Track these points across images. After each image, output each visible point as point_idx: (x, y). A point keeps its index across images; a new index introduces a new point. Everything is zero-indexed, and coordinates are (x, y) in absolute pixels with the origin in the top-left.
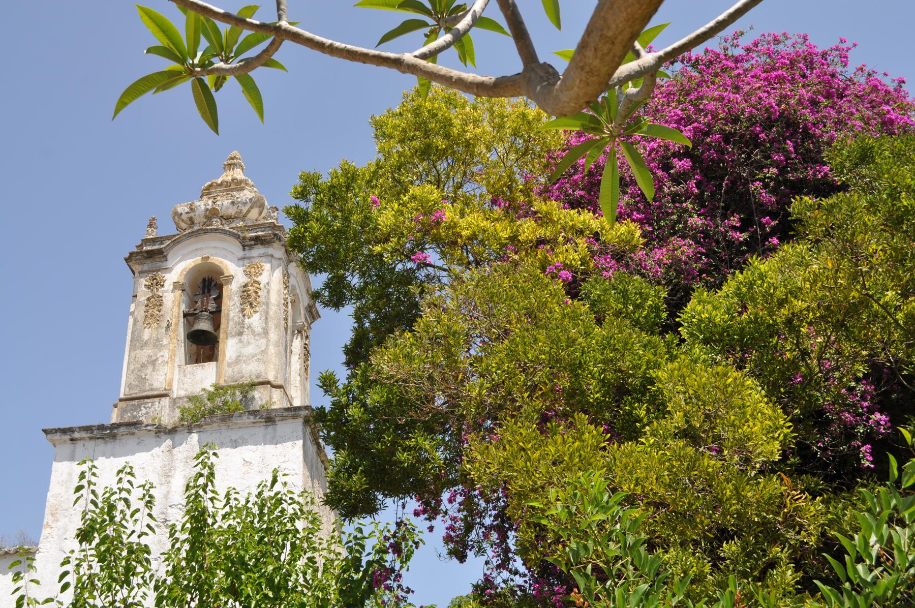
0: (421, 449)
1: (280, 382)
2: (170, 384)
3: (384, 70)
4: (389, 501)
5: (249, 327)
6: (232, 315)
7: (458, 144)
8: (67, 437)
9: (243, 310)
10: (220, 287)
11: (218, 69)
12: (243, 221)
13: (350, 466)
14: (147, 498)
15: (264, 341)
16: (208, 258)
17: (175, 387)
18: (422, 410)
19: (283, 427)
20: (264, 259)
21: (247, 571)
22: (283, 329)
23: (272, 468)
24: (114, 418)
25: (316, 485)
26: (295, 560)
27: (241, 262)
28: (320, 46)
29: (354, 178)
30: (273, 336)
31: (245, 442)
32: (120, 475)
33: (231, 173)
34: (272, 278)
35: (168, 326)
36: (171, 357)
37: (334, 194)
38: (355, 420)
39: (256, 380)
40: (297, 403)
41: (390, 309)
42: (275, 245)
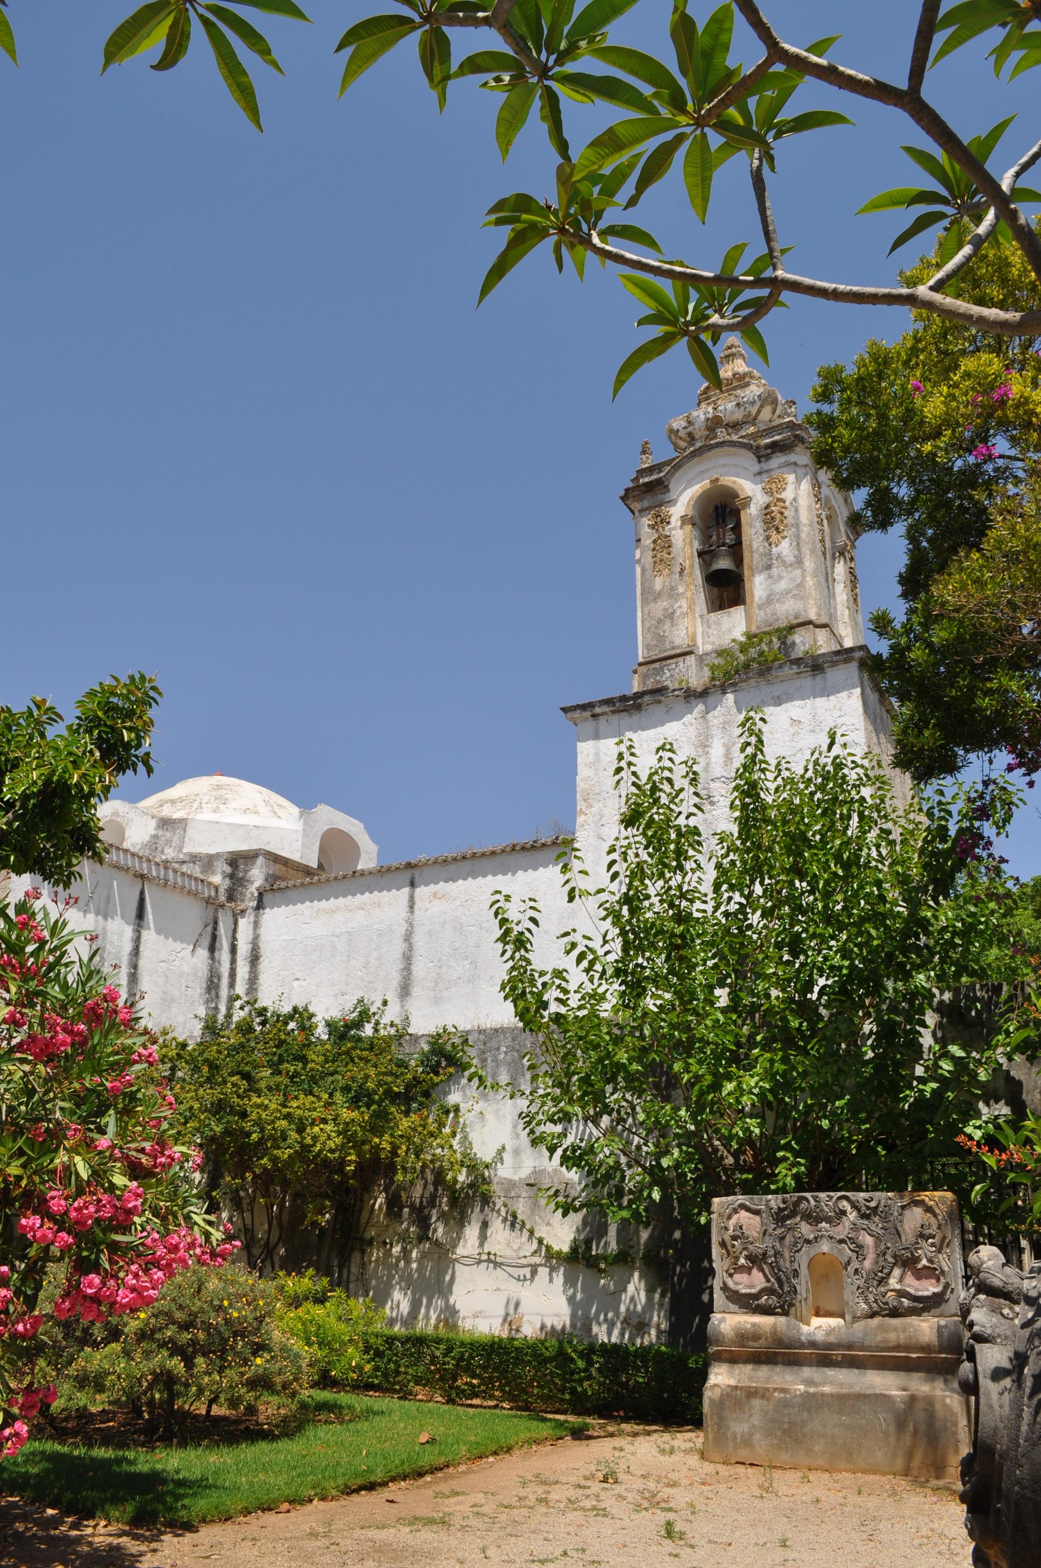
0: (1006, 691)
1: (824, 620)
2: (694, 639)
3: (897, 308)
4: (972, 756)
5: (779, 557)
6: (755, 545)
7: (1020, 289)
8: (588, 714)
9: (768, 538)
10: (736, 513)
11: (714, 326)
12: (754, 425)
13: (920, 720)
14: (691, 775)
15: (798, 572)
16: (717, 479)
17: (700, 642)
18: (1002, 644)
19: (835, 675)
20: (785, 469)
21: (810, 847)
22: (820, 554)
23: (826, 727)
24: (636, 687)
25: (883, 740)
26: (865, 832)
27: (758, 478)
28: (823, 293)
29: (886, 362)
30: (809, 564)
31: (790, 698)
32: (661, 753)
33: (731, 366)
34: (800, 492)
35: (682, 570)
36: (690, 607)
37: (864, 388)
38: (920, 665)
39: (795, 622)
40: (848, 643)
41: (950, 522)
42: (798, 449)
